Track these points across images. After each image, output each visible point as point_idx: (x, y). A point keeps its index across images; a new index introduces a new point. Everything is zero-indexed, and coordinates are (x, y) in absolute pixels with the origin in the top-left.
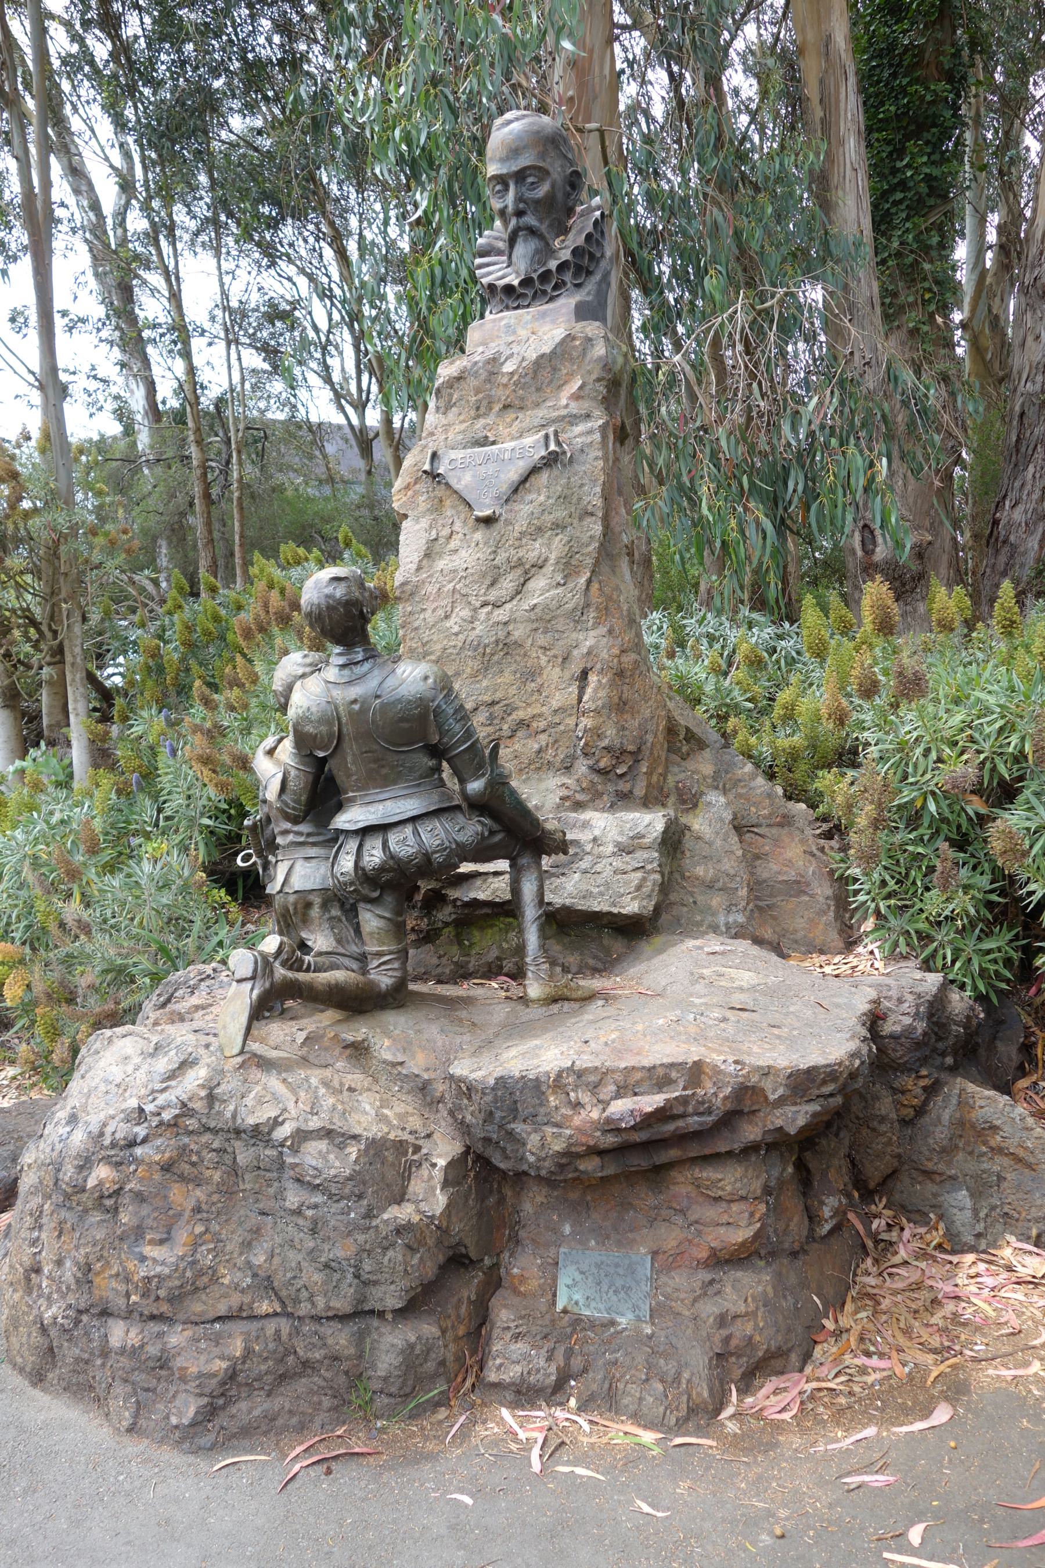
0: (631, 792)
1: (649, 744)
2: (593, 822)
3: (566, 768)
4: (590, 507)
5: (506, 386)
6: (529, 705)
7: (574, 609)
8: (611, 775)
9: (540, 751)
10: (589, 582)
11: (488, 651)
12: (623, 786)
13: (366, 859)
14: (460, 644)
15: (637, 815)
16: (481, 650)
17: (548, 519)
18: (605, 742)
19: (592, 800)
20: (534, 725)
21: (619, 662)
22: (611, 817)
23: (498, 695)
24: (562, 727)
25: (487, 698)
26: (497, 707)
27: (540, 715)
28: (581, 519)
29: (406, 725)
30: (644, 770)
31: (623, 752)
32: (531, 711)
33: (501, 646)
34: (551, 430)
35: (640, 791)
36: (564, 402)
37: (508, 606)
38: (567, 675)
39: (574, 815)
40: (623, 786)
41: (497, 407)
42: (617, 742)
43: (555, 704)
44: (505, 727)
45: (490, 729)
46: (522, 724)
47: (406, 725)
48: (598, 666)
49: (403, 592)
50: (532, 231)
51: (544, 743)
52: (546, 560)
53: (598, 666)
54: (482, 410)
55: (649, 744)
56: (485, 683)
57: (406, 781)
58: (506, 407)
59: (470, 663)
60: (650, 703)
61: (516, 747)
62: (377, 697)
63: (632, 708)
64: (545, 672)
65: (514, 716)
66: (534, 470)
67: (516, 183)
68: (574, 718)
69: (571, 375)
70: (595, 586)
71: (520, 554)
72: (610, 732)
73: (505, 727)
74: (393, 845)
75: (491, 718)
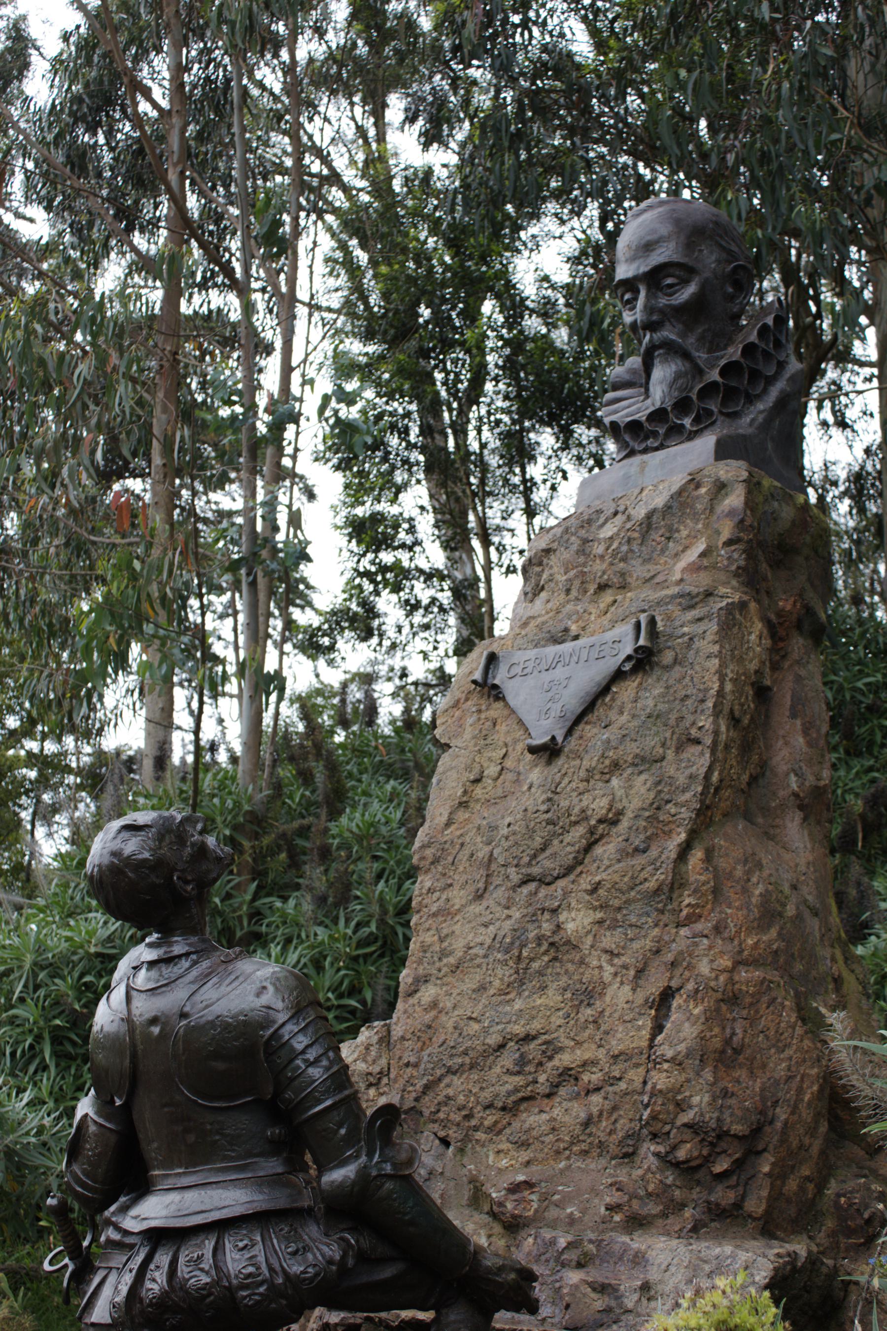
0: (738, 1205)
1: (779, 1125)
2: (651, 1254)
3: (626, 1155)
4: (694, 732)
5: (602, 557)
6: (579, 1044)
7: (657, 891)
8: (701, 1175)
9: (587, 1123)
10: (684, 851)
11: (525, 953)
12: (724, 1196)
13: (149, 1285)
14: (488, 941)
15: (728, 1249)
16: (516, 952)
17: (632, 749)
18: (685, 1118)
19: (664, 1215)
20: (585, 1077)
21: (731, 981)
22: (682, 1249)
23: (536, 1026)
24: (623, 1085)
25: (518, 1029)
26: (533, 1045)
27: (594, 1062)
28: (679, 749)
29: (220, 1066)
30: (766, 1169)
31: (722, 1135)
32: (581, 1055)
33: (545, 946)
34: (643, 618)
35: (755, 1205)
36: (677, 576)
37: (561, 883)
38: (640, 998)
39: (626, 1239)
40: (724, 1196)
41: (592, 588)
42: (711, 1117)
43: (616, 1045)
44: (542, 1078)
45: (518, 1080)
46: (567, 1075)
47: (220, 1066)
48: (690, 986)
49: (423, 858)
50: (671, 349)
51: (595, 1111)
52: (620, 813)
53: (690, 986)
54: (574, 593)
55: (779, 1125)
56: (518, 1005)
57: (226, 1158)
58: (602, 587)
59: (499, 972)
60: (788, 1052)
61: (556, 1111)
62: (183, 1015)
63: (752, 1059)
64: (610, 992)
65: (556, 1062)
66: (618, 675)
67: (648, 291)
68: (641, 1070)
69: (693, 537)
70: (697, 856)
71: (584, 803)
72: (700, 1099)
73: (542, 1078)
74: (183, 1270)
75: (522, 1061)
